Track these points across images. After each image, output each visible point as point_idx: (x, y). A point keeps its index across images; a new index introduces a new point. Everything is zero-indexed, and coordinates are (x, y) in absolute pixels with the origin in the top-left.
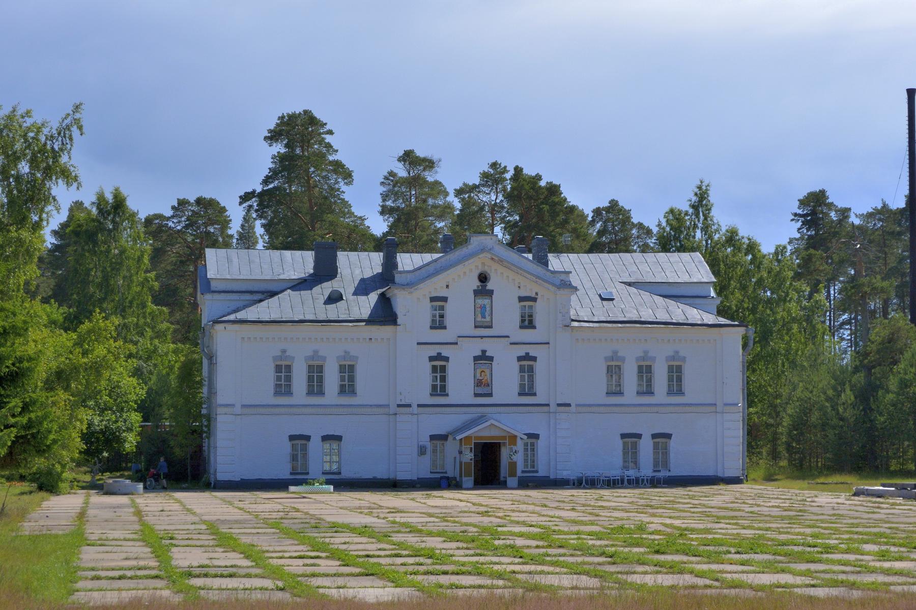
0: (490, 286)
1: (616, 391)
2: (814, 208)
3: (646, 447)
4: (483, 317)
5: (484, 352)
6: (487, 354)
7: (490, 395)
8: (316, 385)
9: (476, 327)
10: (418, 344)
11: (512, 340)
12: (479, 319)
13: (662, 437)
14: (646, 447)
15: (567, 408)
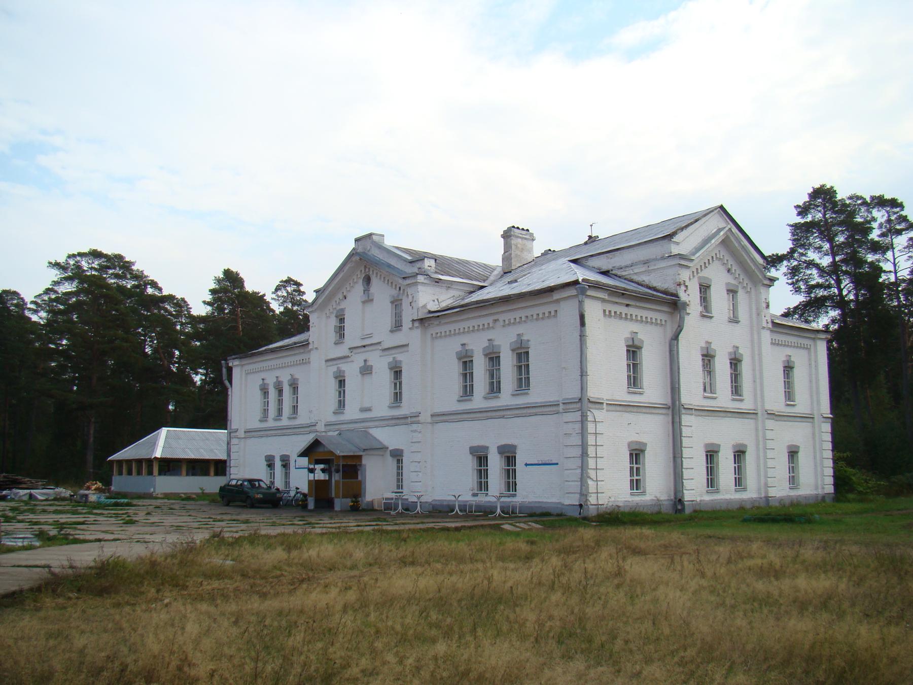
6: (369, 363)
10: (407, 345)
11: (386, 345)
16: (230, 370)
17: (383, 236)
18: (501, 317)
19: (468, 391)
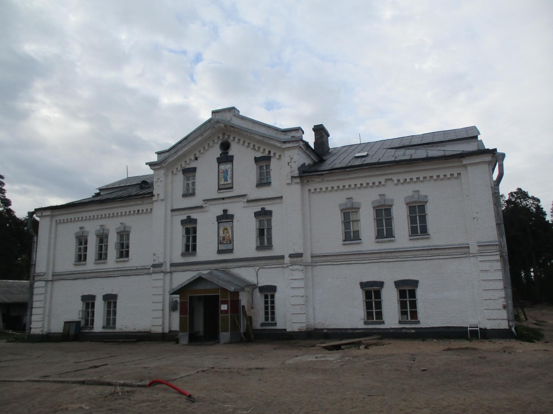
0: (231, 153)
1: (351, 236)
3: (390, 300)
5: (225, 211)
6: (229, 213)
7: (231, 251)
8: (385, 230)
9: (219, 189)
10: (281, 197)
11: (252, 197)
13: (269, 292)
14: (390, 300)
15: (299, 259)
18: (395, 178)
19: (81, 258)
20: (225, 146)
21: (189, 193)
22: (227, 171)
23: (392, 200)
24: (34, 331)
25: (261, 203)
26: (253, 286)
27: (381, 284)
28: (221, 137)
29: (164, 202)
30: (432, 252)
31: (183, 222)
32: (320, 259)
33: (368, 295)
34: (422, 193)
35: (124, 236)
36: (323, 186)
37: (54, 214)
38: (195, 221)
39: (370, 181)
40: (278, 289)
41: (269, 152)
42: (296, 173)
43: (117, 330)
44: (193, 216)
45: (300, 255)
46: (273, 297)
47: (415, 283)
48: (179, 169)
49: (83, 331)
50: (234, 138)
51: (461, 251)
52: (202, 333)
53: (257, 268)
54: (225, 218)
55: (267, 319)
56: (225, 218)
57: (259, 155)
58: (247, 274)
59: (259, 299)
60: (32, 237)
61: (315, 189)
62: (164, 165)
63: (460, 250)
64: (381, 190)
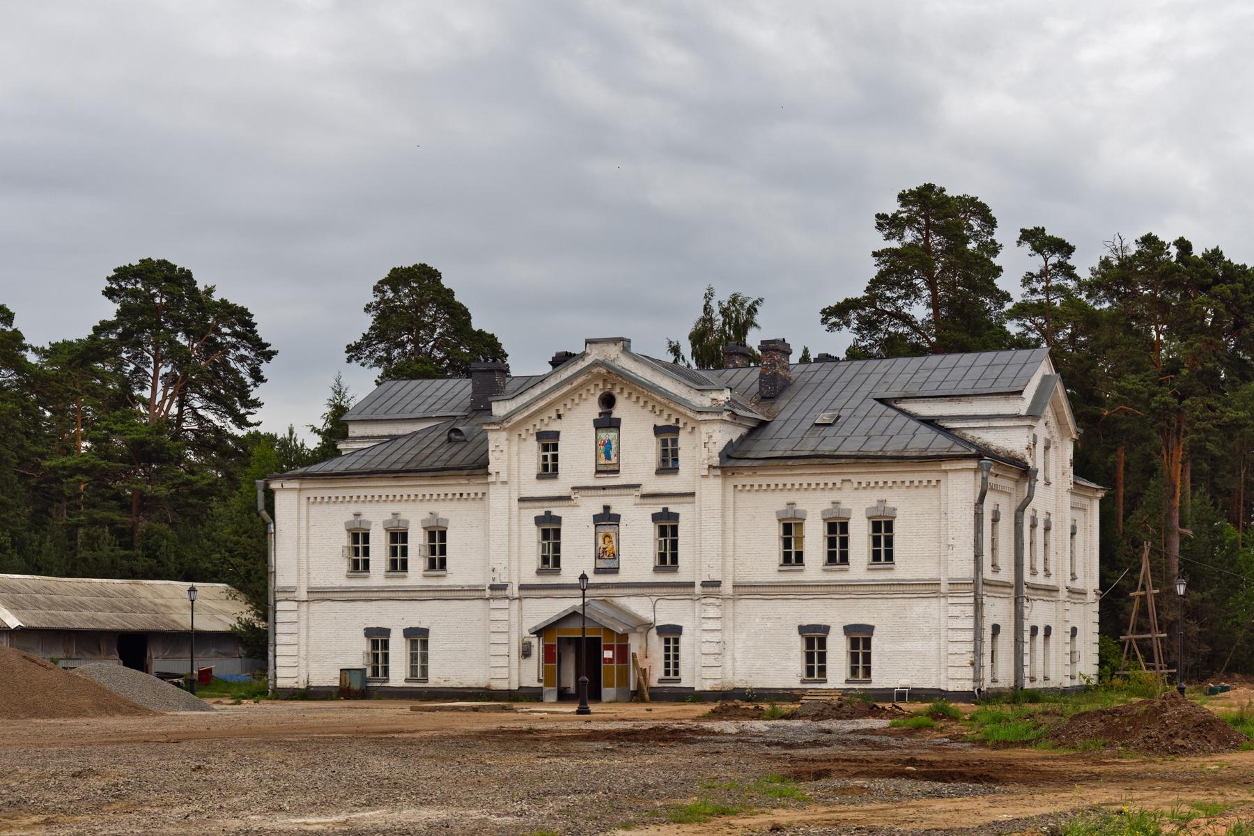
0: (616, 414)
1: (792, 557)
2: (1000, 269)
3: (399, 650)
4: (608, 457)
5: (607, 508)
6: (612, 511)
7: (615, 571)
8: (837, 553)
9: (598, 472)
10: (693, 494)
11: (647, 489)
12: (602, 461)
13: (671, 634)
15: (689, 590)
16: (270, 495)
17: (629, 341)
18: (855, 479)
19: (360, 564)
20: (608, 401)
21: (549, 470)
22: (609, 442)
23: (849, 511)
24: (281, 683)
25: (662, 500)
26: (648, 626)
27: (826, 629)
28: (601, 386)
29: (507, 487)
30: (895, 588)
31: (539, 521)
32: (746, 590)
33: (809, 643)
34: (890, 505)
35: (437, 537)
36: (756, 481)
37: (304, 486)
38: (558, 520)
39: (822, 480)
40: (685, 631)
41: (677, 420)
42: (716, 461)
43: (430, 684)
44: (555, 512)
45: (717, 584)
46: (677, 641)
47: (870, 629)
48: (531, 431)
49: (370, 685)
50: (622, 389)
51: (927, 588)
52: (572, 690)
53: (654, 599)
54: (606, 519)
55: (667, 673)
56: (606, 519)
57: (661, 422)
58: (640, 607)
59: (657, 644)
60: (266, 525)
61: (744, 486)
62: (507, 425)
63: (930, 588)
64: (835, 496)
